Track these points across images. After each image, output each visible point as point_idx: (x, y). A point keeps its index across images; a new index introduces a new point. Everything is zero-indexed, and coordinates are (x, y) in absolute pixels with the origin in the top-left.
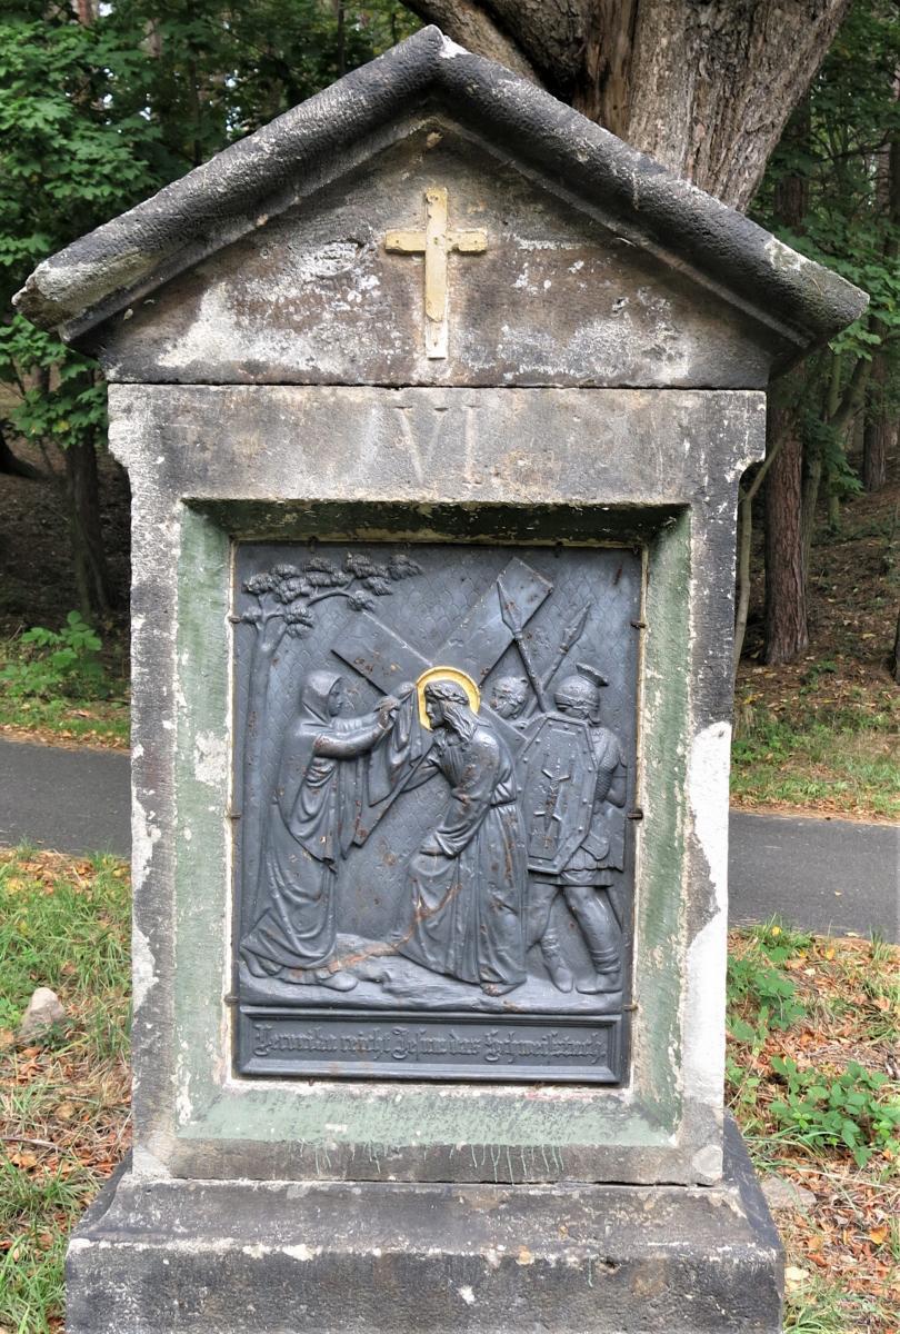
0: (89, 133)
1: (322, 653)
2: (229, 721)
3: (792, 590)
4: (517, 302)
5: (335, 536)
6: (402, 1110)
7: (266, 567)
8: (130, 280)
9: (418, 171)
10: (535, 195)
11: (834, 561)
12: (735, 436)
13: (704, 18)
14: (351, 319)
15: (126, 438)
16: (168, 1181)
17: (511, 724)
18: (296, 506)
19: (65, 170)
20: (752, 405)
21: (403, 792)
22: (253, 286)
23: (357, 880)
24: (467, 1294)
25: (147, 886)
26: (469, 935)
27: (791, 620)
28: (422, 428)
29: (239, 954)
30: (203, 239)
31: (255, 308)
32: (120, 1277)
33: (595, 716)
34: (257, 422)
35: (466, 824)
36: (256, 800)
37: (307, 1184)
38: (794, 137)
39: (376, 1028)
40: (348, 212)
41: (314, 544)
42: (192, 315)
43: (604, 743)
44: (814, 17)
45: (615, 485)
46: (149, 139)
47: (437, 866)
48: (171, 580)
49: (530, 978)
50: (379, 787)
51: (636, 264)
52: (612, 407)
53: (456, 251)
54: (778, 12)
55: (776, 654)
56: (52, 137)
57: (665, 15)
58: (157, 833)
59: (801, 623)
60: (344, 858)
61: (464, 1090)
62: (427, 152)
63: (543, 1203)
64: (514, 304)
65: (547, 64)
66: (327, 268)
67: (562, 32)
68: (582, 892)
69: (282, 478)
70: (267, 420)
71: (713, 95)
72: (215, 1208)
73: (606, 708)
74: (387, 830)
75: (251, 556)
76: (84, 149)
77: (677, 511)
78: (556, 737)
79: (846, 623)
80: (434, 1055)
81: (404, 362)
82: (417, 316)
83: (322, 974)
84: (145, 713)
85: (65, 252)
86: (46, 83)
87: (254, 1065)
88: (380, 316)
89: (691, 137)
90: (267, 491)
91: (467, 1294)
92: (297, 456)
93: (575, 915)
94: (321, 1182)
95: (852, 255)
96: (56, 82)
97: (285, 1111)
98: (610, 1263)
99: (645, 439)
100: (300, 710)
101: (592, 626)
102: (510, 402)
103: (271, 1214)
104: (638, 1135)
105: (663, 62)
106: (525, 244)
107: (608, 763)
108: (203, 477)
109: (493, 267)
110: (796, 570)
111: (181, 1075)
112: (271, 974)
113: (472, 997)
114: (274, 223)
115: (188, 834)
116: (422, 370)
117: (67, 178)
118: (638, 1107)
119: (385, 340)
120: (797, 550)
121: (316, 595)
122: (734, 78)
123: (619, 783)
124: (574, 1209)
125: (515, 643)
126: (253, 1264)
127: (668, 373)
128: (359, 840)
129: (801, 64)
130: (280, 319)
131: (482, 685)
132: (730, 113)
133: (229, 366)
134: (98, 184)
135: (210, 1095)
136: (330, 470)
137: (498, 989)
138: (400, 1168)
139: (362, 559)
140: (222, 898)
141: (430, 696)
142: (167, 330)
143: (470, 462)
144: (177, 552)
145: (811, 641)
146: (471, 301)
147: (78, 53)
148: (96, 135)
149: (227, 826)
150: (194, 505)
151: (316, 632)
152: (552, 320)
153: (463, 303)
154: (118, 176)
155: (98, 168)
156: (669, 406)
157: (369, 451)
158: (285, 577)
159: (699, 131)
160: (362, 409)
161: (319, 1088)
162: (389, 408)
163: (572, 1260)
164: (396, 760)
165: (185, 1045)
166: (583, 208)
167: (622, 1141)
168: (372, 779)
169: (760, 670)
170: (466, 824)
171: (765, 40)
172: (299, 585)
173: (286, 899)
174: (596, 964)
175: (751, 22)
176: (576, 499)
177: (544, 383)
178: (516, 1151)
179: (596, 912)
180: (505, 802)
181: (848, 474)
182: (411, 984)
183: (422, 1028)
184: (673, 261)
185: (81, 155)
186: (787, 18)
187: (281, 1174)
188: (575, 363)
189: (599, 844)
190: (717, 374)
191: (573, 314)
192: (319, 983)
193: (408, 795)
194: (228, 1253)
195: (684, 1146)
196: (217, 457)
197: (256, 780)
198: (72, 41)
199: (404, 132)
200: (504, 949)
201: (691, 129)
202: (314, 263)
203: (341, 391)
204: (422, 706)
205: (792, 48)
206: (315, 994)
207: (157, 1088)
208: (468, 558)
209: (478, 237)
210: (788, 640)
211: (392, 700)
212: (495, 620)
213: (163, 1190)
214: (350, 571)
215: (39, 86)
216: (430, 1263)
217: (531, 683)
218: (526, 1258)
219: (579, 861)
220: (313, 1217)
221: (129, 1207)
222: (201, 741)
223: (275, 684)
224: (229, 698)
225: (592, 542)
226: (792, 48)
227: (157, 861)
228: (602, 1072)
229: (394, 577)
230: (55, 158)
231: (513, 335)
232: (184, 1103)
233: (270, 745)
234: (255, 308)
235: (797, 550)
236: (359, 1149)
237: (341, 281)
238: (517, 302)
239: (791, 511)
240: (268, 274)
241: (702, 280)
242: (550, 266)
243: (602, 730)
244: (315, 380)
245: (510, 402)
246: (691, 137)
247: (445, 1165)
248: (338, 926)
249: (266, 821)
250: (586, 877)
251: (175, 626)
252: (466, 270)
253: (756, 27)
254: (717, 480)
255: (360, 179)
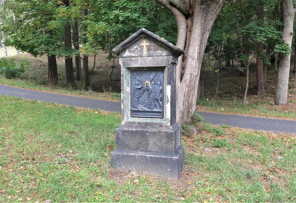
0: (142, 17)
1: (137, 80)
2: (130, 86)
3: (261, 82)
4: (151, 49)
5: (138, 70)
6: (144, 120)
7: (133, 73)
8: (120, 50)
9: (143, 39)
10: (152, 41)
11: (273, 77)
12: (170, 60)
13: (202, 7)
14: (138, 52)
15: (121, 62)
16: (124, 124)
17: (153, 86)
18: (134, 67)
19: (138, 24)
20: (171, 57)
21: (144, 92)
22: (130, 49)
23: (140, 100)
24: (147, 134)
25: (122, 100)
26: (149, 105)
27: (261, 87)
28: (144, 60)
29: (131, 106)
30: (126, 46)
31: (130, 51)
32: (120, 132)
33: (160, 85)
34: (131, 60)
35: (149, 95)
36: (132, 93)
37: (135, 125)
38: (219, 18)
39: (142, 113)
40: (138, 43)
41: (136, 71)
42: (125, 52)
43: (161, 88)
44: (218, 4)
45: (160, 65)
46: (151, 17)
47: (147, 98)
48: (124, 74)
49: (155, 109)
50: (142, 92)
51: (160, 46)
52: (159, 58)
53: (146, 45)
54: (212, 5)
55: (259, 93)
56: (137, 19)
57: (198, 7)
58: (123, 95)
59: (263, 88)
60: (139, 98)
61: (149, 118)
62: (143, 37)
63: (154, 127)
64: (151, 50)
65: (184, 13)
66: (136, 47)
67: (185, 10)
68: (159, 101)
69: (133, 65)
70: (131, 60)
71: (204, 16)
72: (128, 127)
73: (161, 84)
74: (143, 95)
75: (131, 72)
76: (141, 20)
77: (165, 67)
78: (157, 87)
79: (272, 88)
80: (147, 115)
81: (142, 55)
82: (143, 51)
83: (137, 108)
84: (122, 85)
85: (115, 48)
86: (137, 11)
87: (132, 116)
88: (141, 51)
89: (201, 21)
90: (132, 66)
91: (147, 134)
92: (134, 63)
93: (159, 103)
94: (136, 125)
95: (263, 26)
96: (138, 11)
97: (134, 119)
98: (159, 132)
99: (162, 61)
100: (135, 85)
101: (160, 77)
102: (151, 58)
103: (132, 127)
104: (163, 122)
105: (197, 12)
106: (152, 44)
107: (161, 89)
108: (127, 65)
109: (149, 47)
110: (262, 79)
111: (125, 116)
112: (133, 108)
113: (150, 110)
114: (131, 44)
115: (126, 95)
116: (144, 56)
117: (139, 25)
118: (164, 120)
119: (141, 53)
120: (262, 75)
121: (137, 75)
122: (207, 14)
123: (162, 91)
124: (157, 128)
125: (153, 79)
126: (130, 131)
127: (164, 55)
128: (140, 96)
129: (217, 10)
130: (132, 52)
131: (150, 82)
132: (206, 18)
133: (128, 56)
134: (143, 25)
135: (127, 117)
136: (136, 64)
137: (152, 109)
138: (143, 124)
139: (140, 72)
140: (129, 101)
141: (146, 84)
142: (124, 53)
143: (148, 63)
144: (125, 72)
145: (265, 91)
146: (147, 49)
147: (141, 6)
148: (143, 18)
149: (130, 95)
150: (126, 68)
151: (137, 78)
152: (154, 51)
153: (147, 50)
154: (146, 24)
155: (143, 23)
156: (164, 57)
157: (139, 62)
158: (134, 74)
159: (202, 21)
160: (139, 59)
161: (137, 118)
162: (141, 59)
163: (156, 131)
164: (143, 89)
165: (126, 113)
166: (155, 41)
167: (162, 122)
168: (92, 68)
169: (255, 96)
170: (149, 95)
171: (211, 8)
172: (135, 74)
173: (135, 101)
174: (161, 107)
175: (209, 6)
176: (157, 66)
177: (154, 56)
178: (152, 123)
179: (161, 103)
180: (152, 93)
181: (268, 62)
182: (145, 109)
183: (146, 113)
184: (163, 45)
185: (141, 21)
186: (214, 5)
187: (133, 124)
188: (156, 54)
189: (160, 96)
190: (168, 55)
191: (156, 50)
192: (137, 109)
193: (144, 93)
194: (128, 130)
195: (167, 123)
196: (128, 64)
197: (132, 91)
198: (140, 4)
199: (141, 36)
200: (152, 106)
201: (201, 20)
202: (135, 47)
203: (137, 58)
204: (145, 84)
205: (215, 9)
206: (137, 110)
207: (123, 117)
208: (149, 71)
209: (148, 44)
210: (261, 91)
211: (143, 84)
212: (151, 77)
213: (124, 125)
214: (139, 73)
215: (135, 11)
216: (144, 131)
217: (155, 82)
218: (152, 131)
219: (159, 98)
220: (136, 128)
221: (121, 126)
222: (127, 87)
223: (133, 83)
224: (130, 84)
225: (159, 70)
226: (215, 9)
227: (123, 98)
228: (161, 117)
229: (143, 73)
230: (137, 22)
231: (151, 52)
232: (126, 118)
233: (133, 88)
234: (130, 51)
235: (262, 75)
236: (140, 122)
237: (137, 48)
238: (151, 49)
239: (261, 69)
240: (131, 48)
241: (166, 47)
242: (154, 46)
243: (161, 86)
244: (135, 57)
245: (151, 58)
246: (201, 21)
247: (147, 124)
248: (139, 104)
249: (133, 95)
250: (159, 99)
251: (124, 78)
252: (147, 47)
253: (209, 7)
254: (168, 64)
255: (138, 40)
